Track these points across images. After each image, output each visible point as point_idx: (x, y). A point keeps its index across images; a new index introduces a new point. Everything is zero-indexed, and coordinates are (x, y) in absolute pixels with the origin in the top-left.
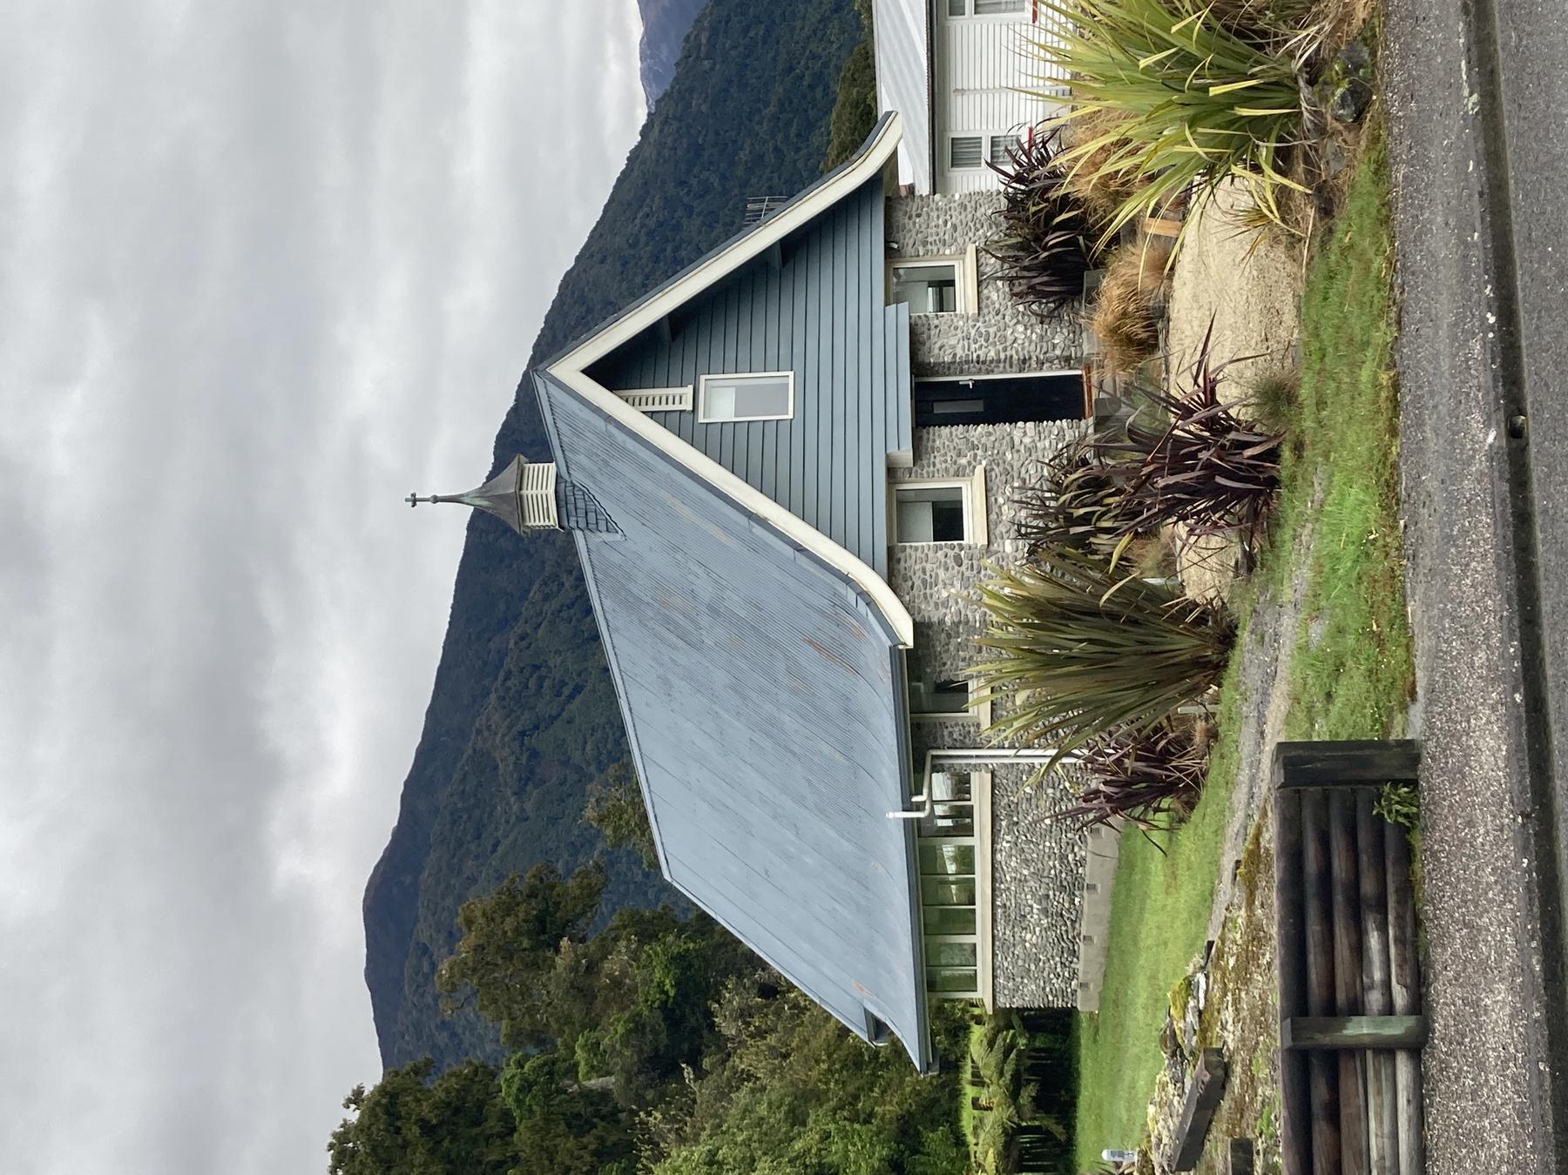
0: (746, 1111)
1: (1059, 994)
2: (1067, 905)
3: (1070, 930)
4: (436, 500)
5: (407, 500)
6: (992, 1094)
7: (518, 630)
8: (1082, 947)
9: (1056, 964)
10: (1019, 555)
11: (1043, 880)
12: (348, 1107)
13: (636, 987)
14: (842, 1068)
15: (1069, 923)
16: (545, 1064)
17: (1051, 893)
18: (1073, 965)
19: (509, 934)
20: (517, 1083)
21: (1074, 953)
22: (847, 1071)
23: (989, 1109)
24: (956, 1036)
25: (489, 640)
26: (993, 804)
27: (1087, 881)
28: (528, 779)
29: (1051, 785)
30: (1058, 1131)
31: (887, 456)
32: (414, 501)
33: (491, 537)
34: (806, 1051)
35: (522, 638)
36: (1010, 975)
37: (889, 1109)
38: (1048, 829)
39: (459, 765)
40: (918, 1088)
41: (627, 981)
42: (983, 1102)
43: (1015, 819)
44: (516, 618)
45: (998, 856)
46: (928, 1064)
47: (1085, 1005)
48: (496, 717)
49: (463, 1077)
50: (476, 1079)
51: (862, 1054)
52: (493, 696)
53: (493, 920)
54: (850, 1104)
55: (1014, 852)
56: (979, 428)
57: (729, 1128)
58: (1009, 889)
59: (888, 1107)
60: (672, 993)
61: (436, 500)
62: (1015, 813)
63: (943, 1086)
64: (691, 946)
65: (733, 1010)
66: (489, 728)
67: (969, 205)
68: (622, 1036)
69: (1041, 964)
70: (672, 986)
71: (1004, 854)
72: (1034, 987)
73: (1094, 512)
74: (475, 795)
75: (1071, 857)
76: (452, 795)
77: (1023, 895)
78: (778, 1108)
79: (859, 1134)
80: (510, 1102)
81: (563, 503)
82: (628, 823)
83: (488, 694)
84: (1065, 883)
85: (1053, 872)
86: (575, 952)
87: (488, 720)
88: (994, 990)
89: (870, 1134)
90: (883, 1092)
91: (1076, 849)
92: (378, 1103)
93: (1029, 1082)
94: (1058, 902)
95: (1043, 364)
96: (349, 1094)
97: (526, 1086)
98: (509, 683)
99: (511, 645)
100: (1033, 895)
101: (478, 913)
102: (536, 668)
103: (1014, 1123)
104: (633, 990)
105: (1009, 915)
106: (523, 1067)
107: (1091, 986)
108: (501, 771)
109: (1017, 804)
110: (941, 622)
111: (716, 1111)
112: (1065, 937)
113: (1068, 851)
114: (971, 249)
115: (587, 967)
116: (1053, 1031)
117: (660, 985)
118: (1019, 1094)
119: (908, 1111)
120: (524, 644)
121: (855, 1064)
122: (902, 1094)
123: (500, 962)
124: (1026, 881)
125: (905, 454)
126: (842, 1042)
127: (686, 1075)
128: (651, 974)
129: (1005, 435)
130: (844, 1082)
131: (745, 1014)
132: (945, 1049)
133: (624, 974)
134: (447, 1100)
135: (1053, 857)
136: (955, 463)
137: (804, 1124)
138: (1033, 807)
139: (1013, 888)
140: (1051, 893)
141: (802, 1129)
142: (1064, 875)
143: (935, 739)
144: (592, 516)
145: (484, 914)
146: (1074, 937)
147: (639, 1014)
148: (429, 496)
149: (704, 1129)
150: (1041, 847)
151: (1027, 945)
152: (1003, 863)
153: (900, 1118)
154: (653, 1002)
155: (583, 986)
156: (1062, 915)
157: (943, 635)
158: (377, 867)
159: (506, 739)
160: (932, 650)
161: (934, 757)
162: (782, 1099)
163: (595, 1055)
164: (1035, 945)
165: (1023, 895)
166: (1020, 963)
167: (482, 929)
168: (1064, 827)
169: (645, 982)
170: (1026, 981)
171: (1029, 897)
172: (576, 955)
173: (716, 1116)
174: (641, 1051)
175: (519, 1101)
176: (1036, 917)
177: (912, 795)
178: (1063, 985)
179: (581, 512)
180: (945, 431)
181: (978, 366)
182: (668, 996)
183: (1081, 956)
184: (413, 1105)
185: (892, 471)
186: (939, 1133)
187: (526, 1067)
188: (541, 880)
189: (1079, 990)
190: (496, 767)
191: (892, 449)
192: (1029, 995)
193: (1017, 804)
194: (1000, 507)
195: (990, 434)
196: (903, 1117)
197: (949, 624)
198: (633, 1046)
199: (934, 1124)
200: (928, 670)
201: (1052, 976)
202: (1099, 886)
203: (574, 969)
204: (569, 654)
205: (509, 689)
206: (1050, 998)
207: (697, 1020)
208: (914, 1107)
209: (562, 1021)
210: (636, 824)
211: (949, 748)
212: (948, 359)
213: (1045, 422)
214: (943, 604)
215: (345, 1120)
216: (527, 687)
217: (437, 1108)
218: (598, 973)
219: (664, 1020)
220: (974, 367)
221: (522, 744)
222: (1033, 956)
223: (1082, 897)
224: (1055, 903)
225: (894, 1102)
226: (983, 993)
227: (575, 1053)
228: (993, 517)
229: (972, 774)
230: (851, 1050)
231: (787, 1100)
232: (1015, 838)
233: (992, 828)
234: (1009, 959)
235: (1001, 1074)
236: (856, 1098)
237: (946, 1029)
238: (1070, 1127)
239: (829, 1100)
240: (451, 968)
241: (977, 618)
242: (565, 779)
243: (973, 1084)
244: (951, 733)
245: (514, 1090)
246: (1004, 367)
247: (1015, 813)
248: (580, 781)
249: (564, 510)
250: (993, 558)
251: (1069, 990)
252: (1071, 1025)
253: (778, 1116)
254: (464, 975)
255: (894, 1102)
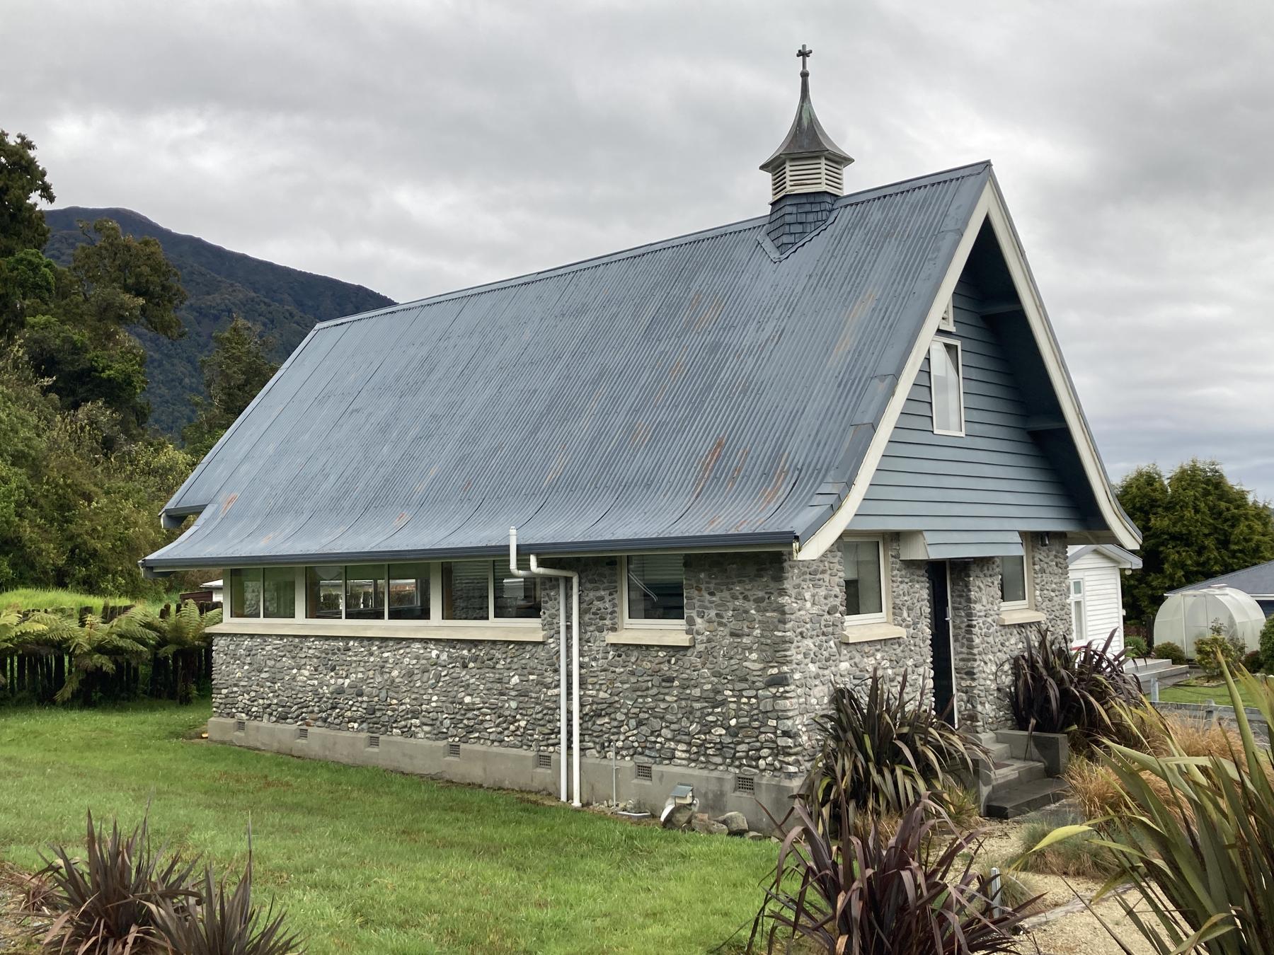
0: (24, 421)
1: (230, 700)
2: (349, 714)
3: (315, 716)
4: (805, 75)
5: (804, 46)
6: (99, 629)
7: (295, 311)
8: (292, 727)
9: (268, 699)
10: (838, 679)
11: (384, 692)
12: (18, 137)
13: (106, 350)
14: (59, 495)
15: (324, 715)
16: (49, 283)
17: (365, 698)
18: (266, 716)
19: (139, 269)
20: (36, 260)
21: (283, 718)
22: (56, 499)
23: (83, 624)
24: (85, 583)
25: (289, 295)
26: (494, 642)
27: (382, 738)
28: (201, 313)
29: (521, 705)
30: (67, 692)
31: (920, 532)
32: (803, 54)
33: (354, 300)
34: (72, 467)
35: (291, 314)
36: (253, 652)
37: (27, 531)
38: (456, 700)
39: (209, 271)
40: (44, 553)
41: (111, 344)
42: (89, 618)
43: (471, 665)
44: (303, 311)
45: (418, 645)
46: (152, 568)
47: (216, 725)
48: (241, 296)
49: (40, 222)
50: (36, 235)
51: (69, 510)
52: (253, 294)
53: (149, 259)
54: (30, 501)
55: (424, 662)
56: (928, 630)
57: (9, 407)
58: (371, 654)
59: (28, 529)
60: (104, 375)
61: (805, 75)
62: (478, 665)
63: (45, 572)
64: (138, 391)
65: (97, 416)
66: (235, 291)
67: (1063, 612)
68: (72, 338)
69: (269, 684)
70: (109, 375)
71: (422, 651)
72: (239, 675)
73: (909, 764)
74: (191, 280)
75: (417, 722)
76: (192, 267)
77: (362, 669)
78: (26, 445)
79: (7, 506)
80: (20, 255)
81: (812, 200)
82: (233, 348)
83: (255, 292)
84: (378, 714)
85: (395, 701)
86: (134, 308)
87: (239, 290)
88: (235, 635)
89: (7, 515)
90: (39, 526)
91: (427, 728)
92: (22, 157)
93: (115, 662)
94: (352, 706)
95: (966, 692)
96: (29, 138)
97: (34, 268)
98: (262, 305)
99: (286, 307)
100: (362, 680)
101: (153, 249)
102: (272, 322)
103: (74, 650)
104: (104, 348)
105: (334, 654)
106: (46, 267)
107: (241, 734)
108: (206, 297)
109: (494, 668)
110: (783, 592)
111: (21, 399)
112: (304, 710)
113: (424, 720)
114: (1040, 616)
115: (122, 316)
116: (153, 681)
117: (110, 368)
118: (103, 654)
119: (25, 545)
120: (287, 315)
121: (61, 505)
122: (39, 541)
123: (117, 263)
124: (382, 673)
125: (918, 552)
126: (79, 496)
127: (46, 379)
128: (117, 361)
129: (924, 657)
130: (47, 496)
131: (93, 422)
132: (74, 575)
133: (116, 343)
134: (23, 209)
135: (415, 702)
136: (903, 605)
137: (13, 464)
138: (489, 685)
139: (372, 659)
140: (365, 698)
141: (9, 462)
142: (390, 713)
143: (589, 586)
144: (799, 228)
145: (152, 253)
146: (303, 719)
147: (86, 351)
148: (808, 68)
149: (7, 388)
150: (430, 691)
151: (295, 671)
152: (408, 650)
153: (19, 539)
154: (96, 362)
155: (109, 312)
156: (334, 708)
157: (761, 594)
158: (146, 218)
159: (227, 301)
160: (735, 580)
161: (568, 581)
162: (33, 449)
163: (42, 329)
164: (294, 678)
165: (362, 669)
166: (271, 663)
167: (142, 250)
168: (458, 717)
169: (111, 356)
170: (246, 667)
171: (360, 675)
172: (132, 309)
173: (18, 399)
174: (59, 351)
175: (20, 261)
176: (332, 681)
177: (537, 555)
178: (241, 705)
179: (802, 218)
180: (925, 594)
181: (963, 626)
182: (101, 372)
183: (279, 726)
184: (20, 183)
185: (896, 537)
186: (8, 570)
187: (46, 269)
188: (175, 295)
189: (233, 721)
190: (209, 294)
191: (929, 537)
192: (225, 668)
193: (494, 668)
194: (873, 655)
195: (924, 641)
196: (20, 541)
197: (781, 600)
198: (63, 346)
199: (13, 565)
200: (702, 576)
201: (253, 694)
202: (376, 750)
203: (122, 306)
204: (280, 342)
205: (259, 305)
206: (224, 691)
207: (81, 393)
208: (28, 550)
209: (67, 307)
210: (234, 353)
211: (580, 595)
212: (973, 595)
213: (933, 699)
214: (799, 594)
215: (7, 135)
216: (260, 315)
217: (17, 200)
218: (119, 324)
219: (83, 370)
220: (963, 622)
221: (223, 311)
222: (278, 676)
223: (358, 731)
224: (351, 703)
225: (32, 535)
226: (229, 624)
227: (43, 315)
228: (867, 649)
229: (539, 620)
230: (73, 503)
231: (33, 453)
232: (443, 663)
233: (459, 641)
234: (275, 652)
235: (121, 636)
236: (35, 506)
237: (90, 575)
238: (68, 705)
239: (33, 484)
240: (113, 229)
241: (788, 634)
242: (200, 336)
243: (105, 608)
244: (601, 599)
245: (30, 258)
246: (961, 653)
247: (478, 665)
248: (199, 345)
249: (804, 200)
250: (835, 650)
251: (234, 710)
252: (160, 698)
253: (20, 445)
254: (108, 237)
255: (32, 535)
